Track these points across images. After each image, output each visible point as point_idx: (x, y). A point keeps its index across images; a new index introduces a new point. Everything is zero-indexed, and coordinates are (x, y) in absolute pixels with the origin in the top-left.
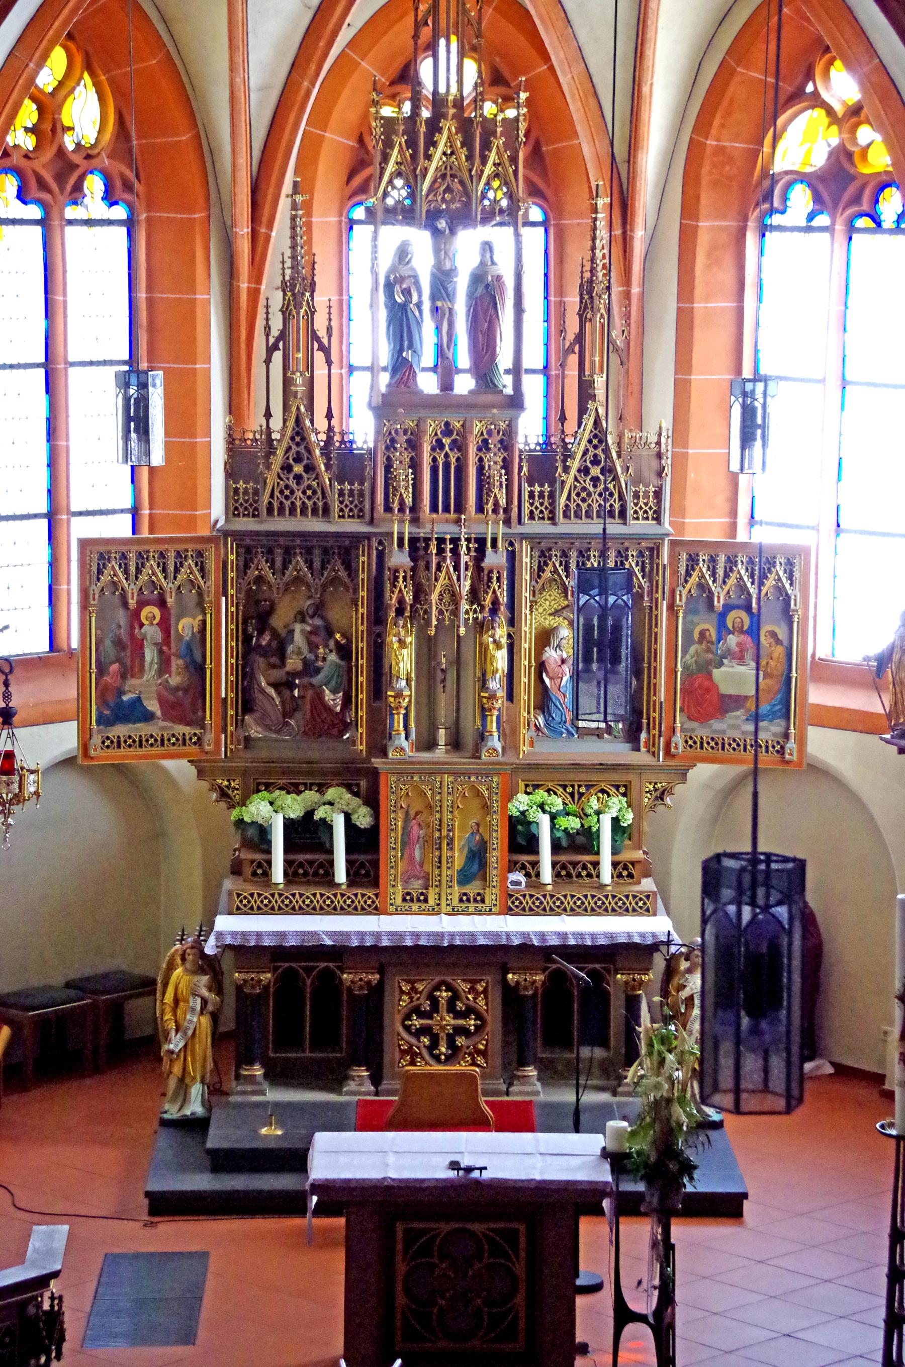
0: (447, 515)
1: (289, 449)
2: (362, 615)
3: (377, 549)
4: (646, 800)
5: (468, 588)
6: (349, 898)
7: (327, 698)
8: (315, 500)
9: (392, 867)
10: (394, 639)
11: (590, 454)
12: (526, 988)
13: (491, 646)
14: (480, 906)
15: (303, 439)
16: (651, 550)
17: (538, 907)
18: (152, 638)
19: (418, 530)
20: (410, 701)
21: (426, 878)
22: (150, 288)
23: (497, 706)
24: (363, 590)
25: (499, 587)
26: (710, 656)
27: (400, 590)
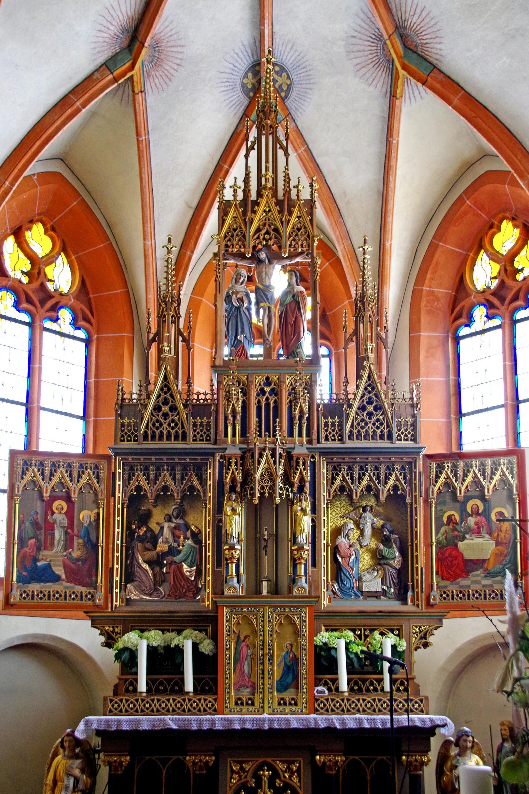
1: (159, 396)
3: (219, 461)
4: (414, 639)
6: (194, 702)
7: (185, 571)
10: (229, 508)
11: (366, 397)
12: (330, 768)
14: (294, 708)
15: (169, 389)
16: (410, 463)
17: (338, 708)
18: (60, 523)
21: (253, 686)
22: (97, 376)
23: (304, 556)
24: (210, 492)
25: (304, 469)
26: (456, 533)
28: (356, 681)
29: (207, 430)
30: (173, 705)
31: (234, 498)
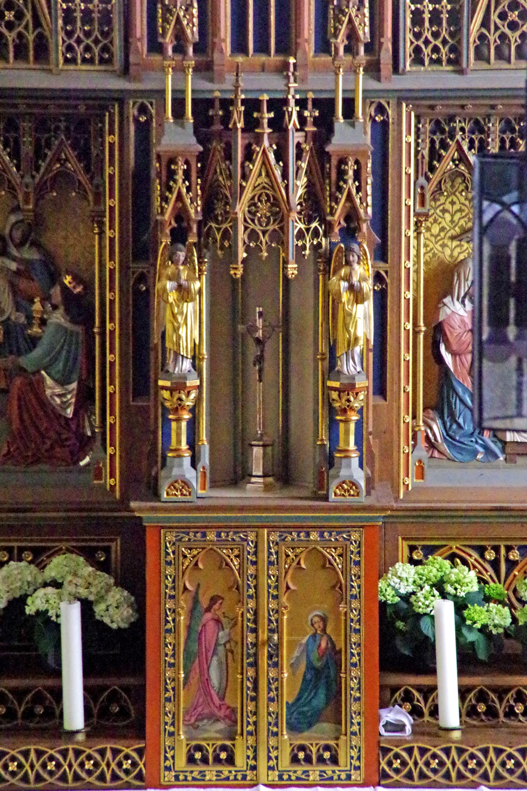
0: (263, 58)
2: (112, 240)
3: (136, 120)
5: (301, 191)
6: (89, 757)
7: (48, 392)
8: (20, 29)
9: (168, 700)
13: (345, 297)
14: (329, 769)
17: (435, 771)
19: (208, 86)
20: (199, 399)
23: (357, 405)
24: (112, 196)
25: (358, 189)
27: (180, 197)
28: (481, 691)
29: (102, 33)
30: (37, 766)
31: (182, 258)
